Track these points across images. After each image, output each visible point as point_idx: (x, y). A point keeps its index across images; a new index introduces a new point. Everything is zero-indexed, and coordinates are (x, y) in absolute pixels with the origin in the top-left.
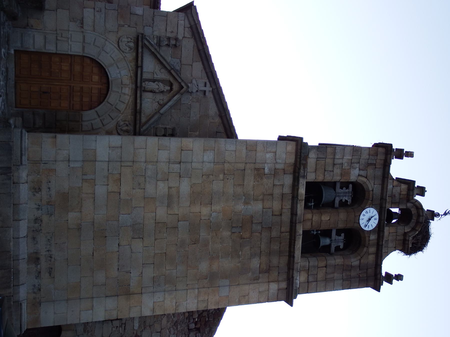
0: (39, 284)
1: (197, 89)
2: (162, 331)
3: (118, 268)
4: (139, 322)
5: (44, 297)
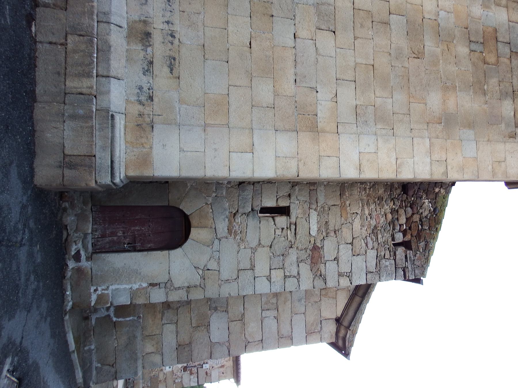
0: (150, 86)
1: (176, 286)
2: (354, 241)
3: (295, 79)
4: (318, 222)
5: (159, 115)
